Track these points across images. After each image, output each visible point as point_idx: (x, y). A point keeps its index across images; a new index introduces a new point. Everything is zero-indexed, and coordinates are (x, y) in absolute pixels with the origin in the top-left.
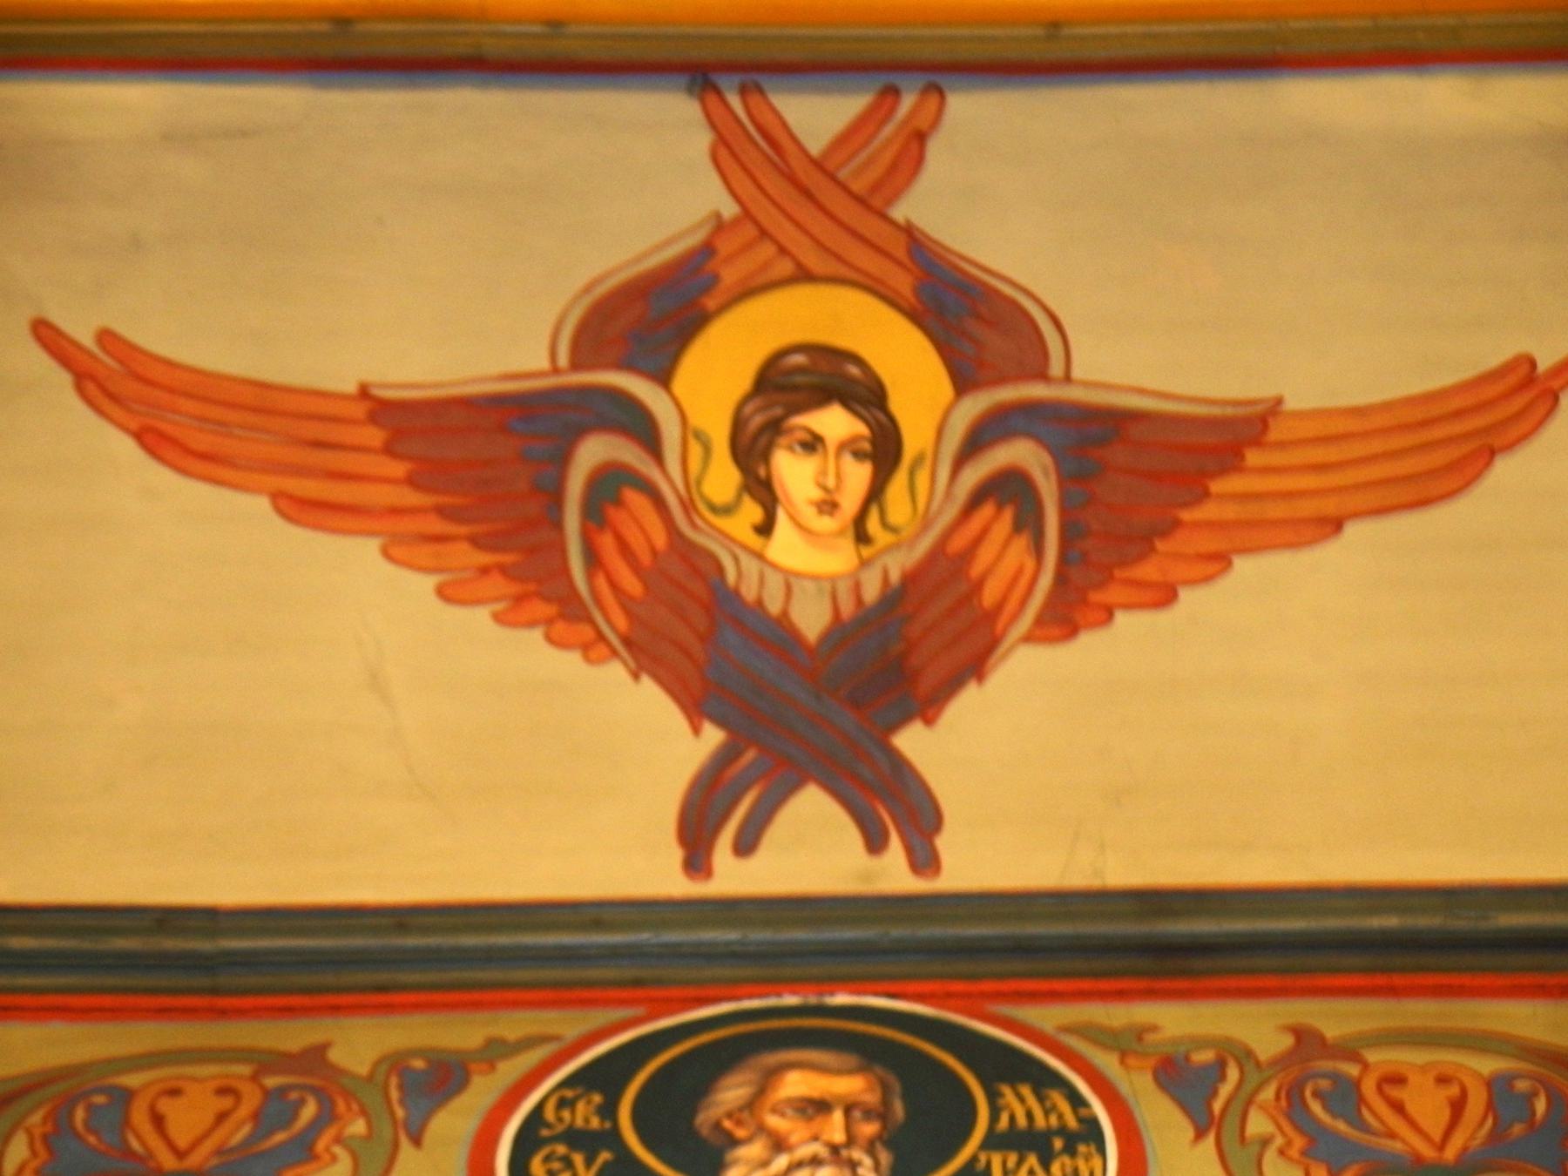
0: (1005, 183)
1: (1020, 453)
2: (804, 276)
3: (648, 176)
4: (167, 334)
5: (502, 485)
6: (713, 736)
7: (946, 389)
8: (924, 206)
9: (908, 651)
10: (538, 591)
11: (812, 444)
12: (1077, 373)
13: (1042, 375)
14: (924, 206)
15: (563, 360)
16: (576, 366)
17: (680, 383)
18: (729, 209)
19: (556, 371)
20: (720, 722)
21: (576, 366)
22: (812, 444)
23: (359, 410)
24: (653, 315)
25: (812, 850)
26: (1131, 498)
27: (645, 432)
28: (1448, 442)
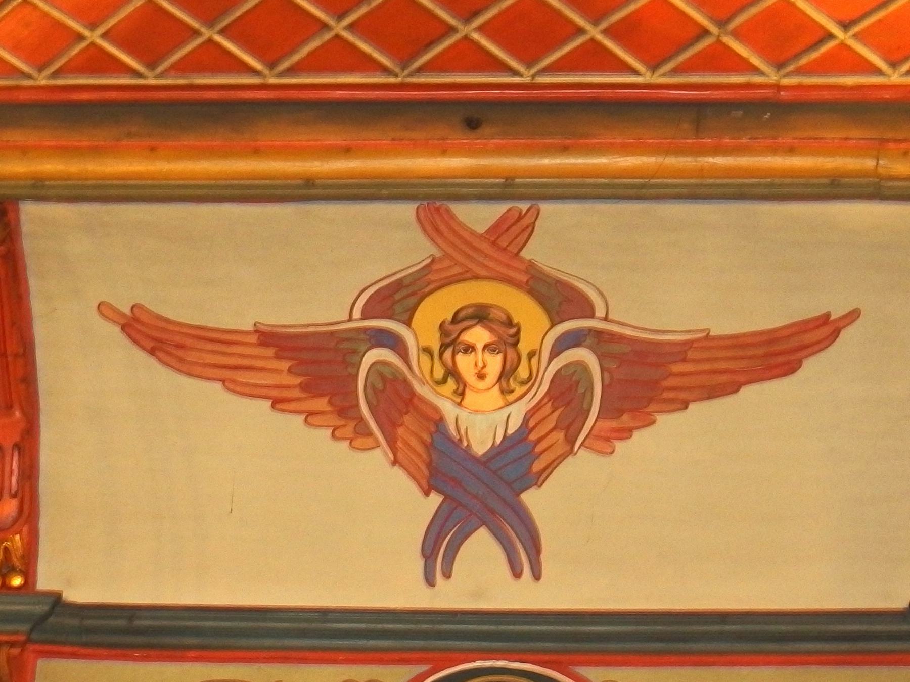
0: (564, 238)
1: (583, 354)
2: (476, 277)
3: (392, 241)
4: (181, 306)
5: (315, 372)
6: (435, 499)
7: (546, 323)
8: (536, 251)
9: (518, 463)
10: (344, 419)
11: (469, 349)
12: (611, 317)
13: (592, 316)
14: (536, 251)
15: (357, 314)
16: (365, 317)
17: (414, 324)
18: (438, 254)
19: (350, 319)
20: (439, 491)
21: (365, 317)
22: (469, 349)
23: (254, 339)
24: (396, 298)
25: (483, 579)
26: (649, 379)
27: (396, 343)
28: (777, 354)
